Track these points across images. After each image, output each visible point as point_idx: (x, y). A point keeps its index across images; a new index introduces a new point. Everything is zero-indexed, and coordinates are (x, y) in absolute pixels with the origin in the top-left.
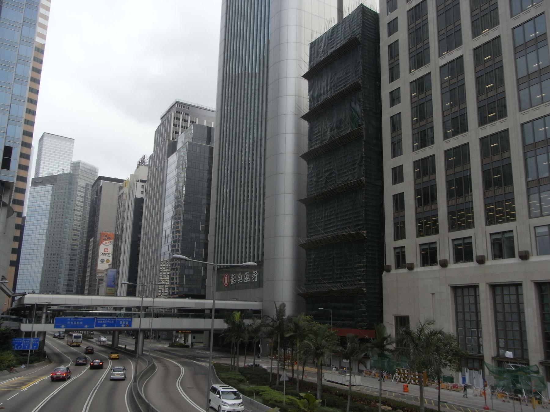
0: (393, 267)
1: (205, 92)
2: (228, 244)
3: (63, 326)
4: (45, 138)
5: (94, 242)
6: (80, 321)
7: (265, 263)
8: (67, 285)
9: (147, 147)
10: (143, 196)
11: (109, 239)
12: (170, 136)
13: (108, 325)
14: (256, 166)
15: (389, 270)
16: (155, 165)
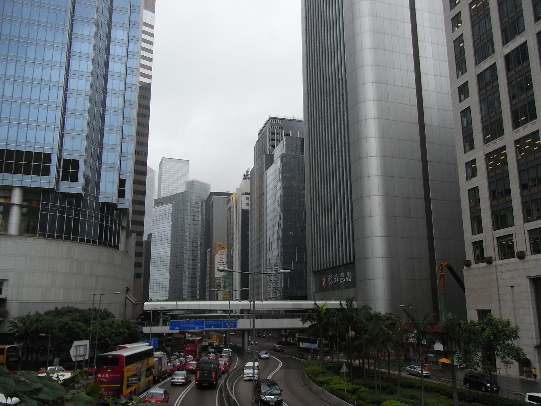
0: (473, 261)
1: (292, 106)
2: (329, 245)
3: (177, 328)
4: (163, 162)
5: (211, 252)
7: (357, 262)
8: (192, 292)
9: (248, 163)
10: (249, 208)
11: (223, 248)
12: (267, 150)
13: (216, 326)
15: (468, 264)
16: (255, 178)
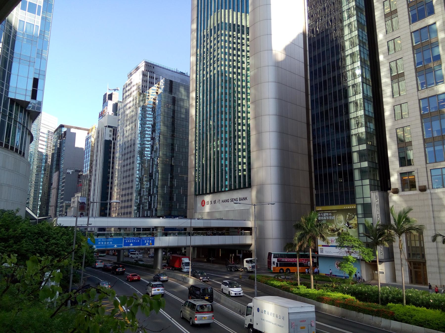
6: (110, 241)
13: (134, 244)
14: (199, 113)
